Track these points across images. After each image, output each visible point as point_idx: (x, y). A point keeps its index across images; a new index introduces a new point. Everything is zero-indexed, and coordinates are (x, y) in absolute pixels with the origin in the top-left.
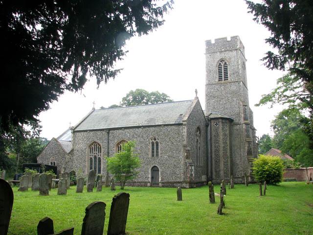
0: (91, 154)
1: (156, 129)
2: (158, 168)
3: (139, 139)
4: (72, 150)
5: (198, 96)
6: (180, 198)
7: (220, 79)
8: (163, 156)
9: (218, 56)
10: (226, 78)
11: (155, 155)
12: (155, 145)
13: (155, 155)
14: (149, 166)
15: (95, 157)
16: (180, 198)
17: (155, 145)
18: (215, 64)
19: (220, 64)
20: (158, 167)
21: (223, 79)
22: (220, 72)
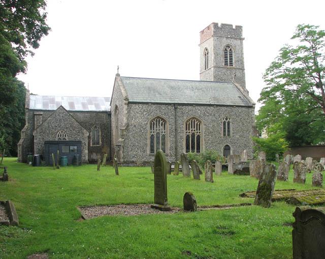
0: (188, 131)
1: (228, 109)
2: (229, 147)
3: (210, 117)
4: (128, 125)
6: (98, 169)
7: (226, 64)
8: (235, 135)
9: (225, 42)
10: (231, 64)
11: (227, 135)
12: (226, 124)
13: (227, 135)
14: (221, 145)
15: (193, 135)
16: (117, 173)
17: (226, 126)
18: (222, 48)
19: (226, 49)
20: (230, 146)
21: (229, 64)
22: (226, 57)
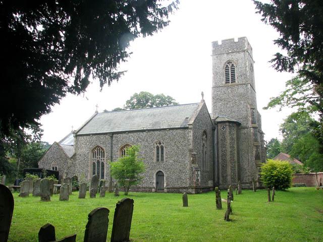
0: (94, 159)
1: (161, 132)
2: (163, 173)
3: (143, 143)
4: (75, 155)
6: (185, 204)
7: (227, 81)
8: (169, 160)
9: (225, 58)
10: (233, 80)
11: (160, 160)
12: (160, 149)
13: (160, 160)
14: (154, 171)
15: (98, 162)
16: (185, 204)
17: (160, 150)
18: (222, 66)
19: (227, 66)
20: (164, 172)
21: (230, 81)
22: (227, 74)
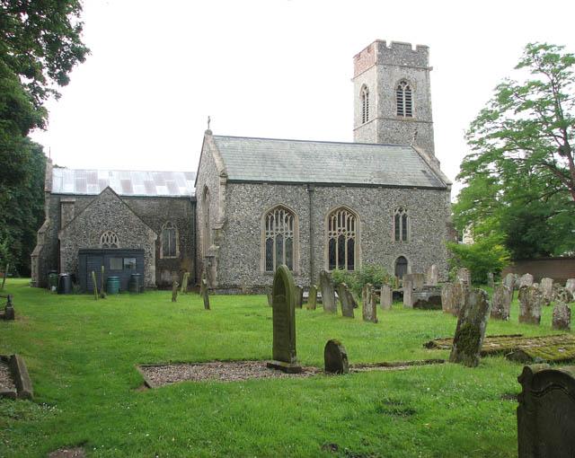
0: (333, 232)
1: (404, 193)
2: (406, 260)
3: (372, 207)
4: (226, 222)
5: (212, 129)
6: (174, 299)
7: (400, 112)
8: (416, 239)
9: (398, 74)
10: (409, 113)
11: (401, 238)
12: (401, 219)
13: (401, 238)
14: (391, 257)
15: (342, 238)
16: (207, 306)
17: (401, 223)
18: (393, 85)
19: (400, 87)
20: (407, 258)
21: (405, 114)
22: (400, 101)
